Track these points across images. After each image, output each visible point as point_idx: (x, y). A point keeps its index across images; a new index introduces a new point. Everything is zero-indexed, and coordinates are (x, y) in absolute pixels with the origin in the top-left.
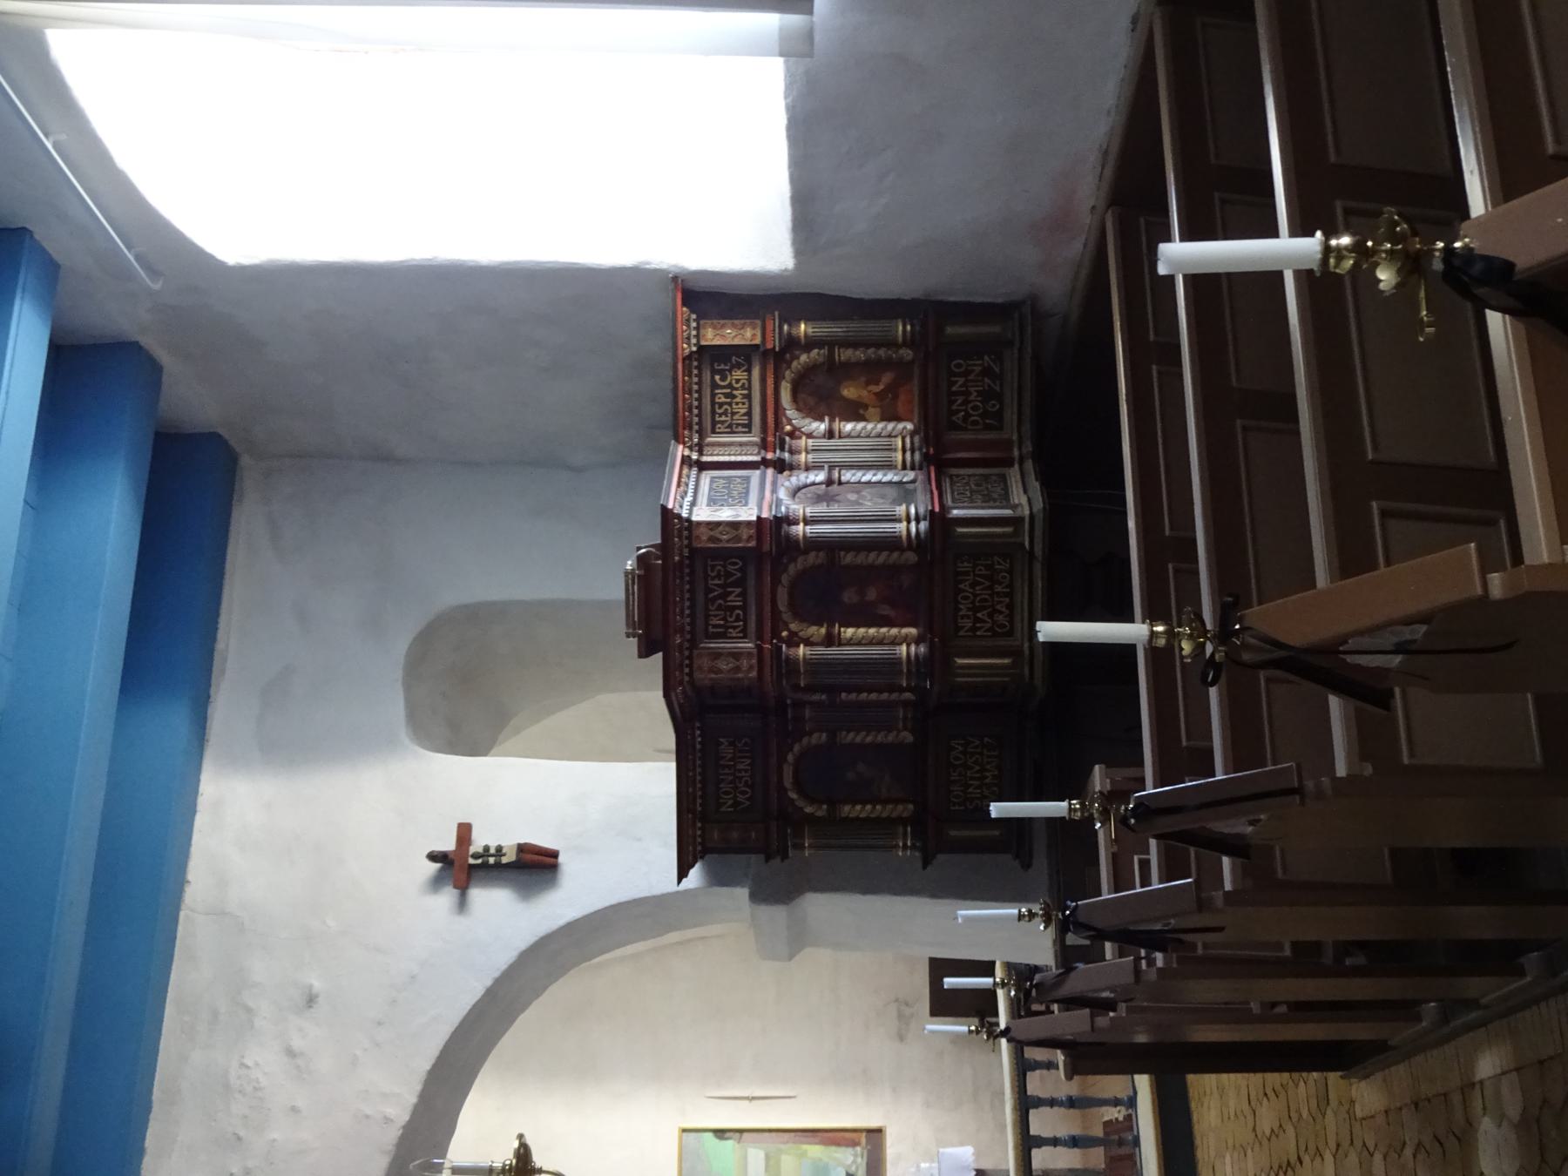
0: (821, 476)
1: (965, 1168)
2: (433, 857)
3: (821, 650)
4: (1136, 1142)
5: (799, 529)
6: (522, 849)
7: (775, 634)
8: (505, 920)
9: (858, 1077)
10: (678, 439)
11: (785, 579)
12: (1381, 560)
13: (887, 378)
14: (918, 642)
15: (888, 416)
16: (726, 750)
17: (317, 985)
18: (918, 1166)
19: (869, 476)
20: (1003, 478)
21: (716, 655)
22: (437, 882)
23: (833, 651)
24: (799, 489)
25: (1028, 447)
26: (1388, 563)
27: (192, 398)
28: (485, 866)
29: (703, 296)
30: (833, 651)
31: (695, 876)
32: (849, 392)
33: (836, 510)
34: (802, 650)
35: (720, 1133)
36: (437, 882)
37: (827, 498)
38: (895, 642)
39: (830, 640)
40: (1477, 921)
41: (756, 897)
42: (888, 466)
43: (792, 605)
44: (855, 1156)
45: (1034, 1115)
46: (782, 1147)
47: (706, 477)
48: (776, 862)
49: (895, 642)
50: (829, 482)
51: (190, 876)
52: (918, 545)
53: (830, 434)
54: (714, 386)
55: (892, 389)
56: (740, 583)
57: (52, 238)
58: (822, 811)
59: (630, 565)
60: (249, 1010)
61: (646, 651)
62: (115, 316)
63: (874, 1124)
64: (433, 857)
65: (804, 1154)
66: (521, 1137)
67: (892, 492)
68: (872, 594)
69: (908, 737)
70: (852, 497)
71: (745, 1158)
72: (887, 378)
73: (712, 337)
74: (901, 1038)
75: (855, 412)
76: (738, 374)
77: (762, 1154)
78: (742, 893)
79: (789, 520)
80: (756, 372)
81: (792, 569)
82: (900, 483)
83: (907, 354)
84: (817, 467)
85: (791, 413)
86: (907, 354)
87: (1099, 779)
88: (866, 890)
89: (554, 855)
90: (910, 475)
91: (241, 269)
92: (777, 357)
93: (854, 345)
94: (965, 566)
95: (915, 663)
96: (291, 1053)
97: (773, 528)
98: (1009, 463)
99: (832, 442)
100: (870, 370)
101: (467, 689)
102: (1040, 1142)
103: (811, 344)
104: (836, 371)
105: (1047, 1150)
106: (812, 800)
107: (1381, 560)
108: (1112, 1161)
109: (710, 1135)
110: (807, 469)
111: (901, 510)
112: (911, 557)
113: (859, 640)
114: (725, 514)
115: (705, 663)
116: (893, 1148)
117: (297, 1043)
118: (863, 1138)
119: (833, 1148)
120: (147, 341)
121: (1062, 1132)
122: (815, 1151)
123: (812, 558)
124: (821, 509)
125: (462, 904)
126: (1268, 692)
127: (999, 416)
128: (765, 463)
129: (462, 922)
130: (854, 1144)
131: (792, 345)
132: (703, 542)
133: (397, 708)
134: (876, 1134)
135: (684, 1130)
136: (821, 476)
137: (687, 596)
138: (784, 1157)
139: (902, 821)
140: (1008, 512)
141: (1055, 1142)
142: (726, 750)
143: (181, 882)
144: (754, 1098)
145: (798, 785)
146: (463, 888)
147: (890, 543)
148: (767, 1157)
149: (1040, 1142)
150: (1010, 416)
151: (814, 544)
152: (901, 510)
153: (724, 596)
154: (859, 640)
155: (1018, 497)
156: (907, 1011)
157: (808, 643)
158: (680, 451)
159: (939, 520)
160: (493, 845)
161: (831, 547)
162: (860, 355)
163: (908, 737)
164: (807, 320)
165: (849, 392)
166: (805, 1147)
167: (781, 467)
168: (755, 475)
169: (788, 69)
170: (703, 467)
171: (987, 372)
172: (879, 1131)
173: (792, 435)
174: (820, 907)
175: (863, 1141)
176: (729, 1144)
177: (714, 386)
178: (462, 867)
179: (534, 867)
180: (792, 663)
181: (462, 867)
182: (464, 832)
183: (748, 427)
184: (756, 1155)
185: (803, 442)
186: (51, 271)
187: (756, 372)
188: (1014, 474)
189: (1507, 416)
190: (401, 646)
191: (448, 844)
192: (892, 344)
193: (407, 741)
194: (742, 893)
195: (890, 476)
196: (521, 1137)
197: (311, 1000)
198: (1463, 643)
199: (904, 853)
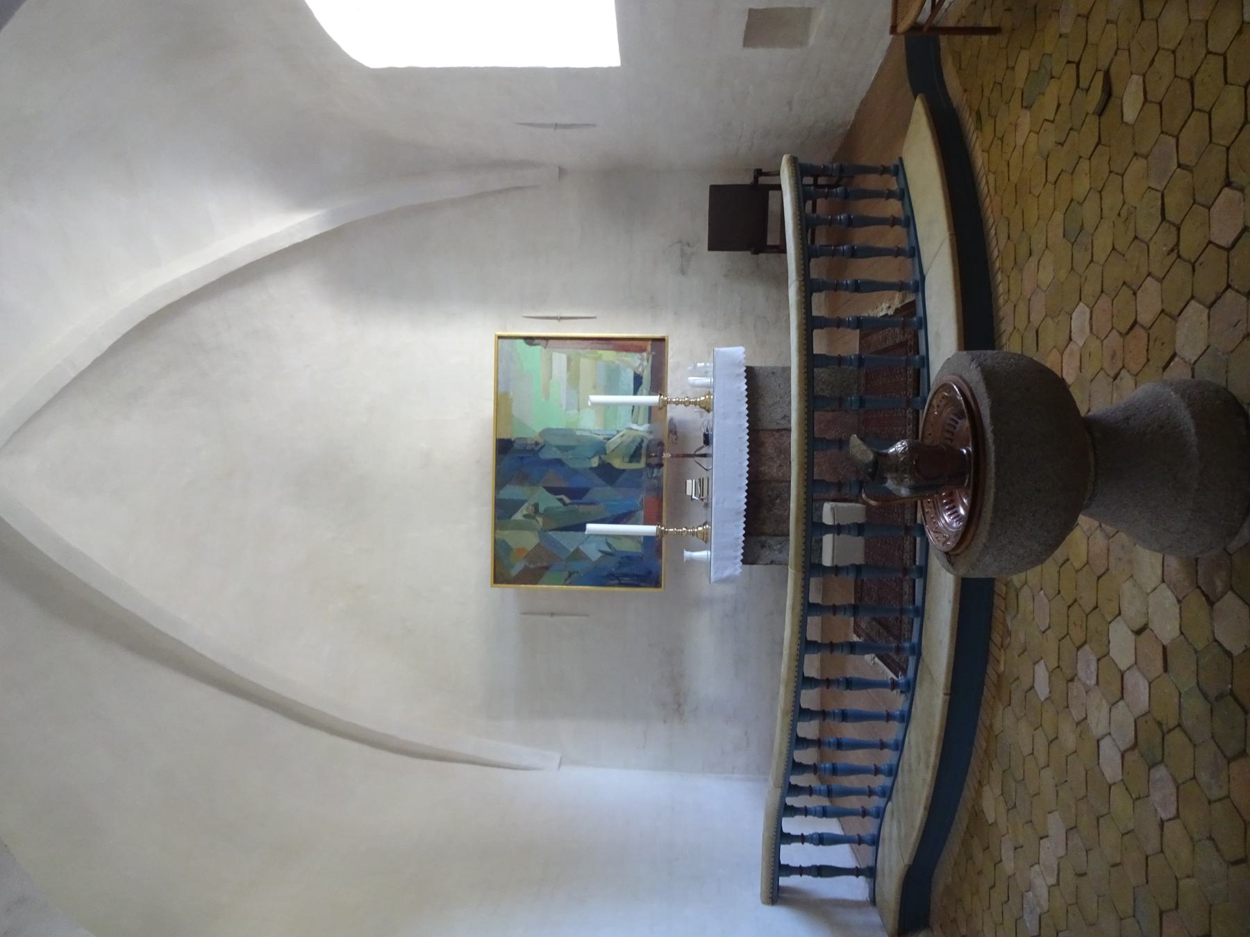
1: (739, 365)
9: (651, 303)
18: (695, 366)
35: (530, 340)
40: (1132, 225)
44: (642, 359)
45: (784, 849)
46: (581, 352)
63: (658, 335)
65: (600, 358)
71: (551, 359)
74: (683, 272)
77: (564, 357)
105: (796, 846)
109: (522, 341)
119: (624, 353)
122: (609, 355)
130: (641, 350)
134: (660, 342)
135: (500, 337)
138: (582, 360)
144: (562, 318)
148: (569, 360)
156: (688, 250)
166: (601, 352)
172: (662, 340)
175: (649, 348)
176: (537, 349)
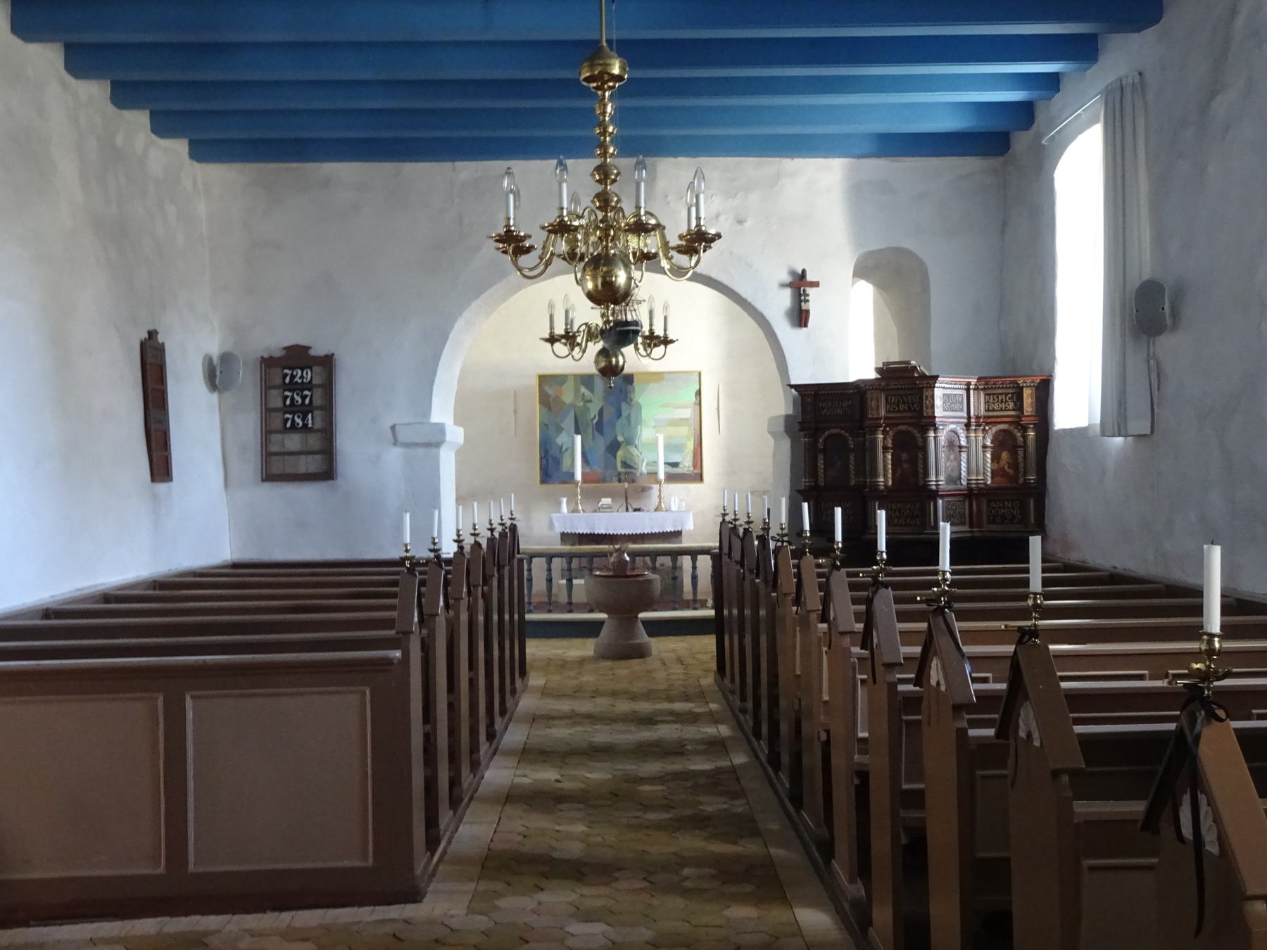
2: (804, 271)
3: (881, 445)
4: (695, 609)
5: (932, 434)
6: (808, 312)
7: (887, 425)
8: (777, 304)
10: (979, 379)
11: (911, 429)
13: (1010, 471)
14: (886, 486)
15: (993, 472)
16: (846, 404)
17: (747, 224)
19: (964, 464)
20: (963, 524)
22: (793, 273)
24: (956, 433)
25: (976, 534)
27: (1021, 141)
28: (800, 295)
29: (1044, 389)
32: (1005, 455)
34: (881, 436)
35: (699, 393)
36: (793, 273)
38: (885, 476)
39: (885, 448)
41: (787, 417)
42: (969, 472)
43: (901, 432)
47: (964, 393)
48: (798, 427)
49: (885, 476)
50: (960, 447)
51: (796, 160)
52: (926, 486)
53: (984, 447)
54: (1006, 394)
55: (1005, 474)
56: (909, 410)
58: (820, 446)
59: (913, 363)
60: (736, 195)
61: (878, 370)
62: (1040, 117)
64: (804, 271)
66: (719, 236)
67: (955, 474)
68: (905, 466)
69: (853, 482)
70: (952, 457)
72: (1010, 471)
73: (1027, 393)
75: (995, 458)
76: (1012, 405)
78: (791, 412)
79: (936, 430)
80: (1012, 413)
81: (1015, 431)
82: (960, 478)
83: (1021, 481)
84: (968, 442)
85: (994, 429)
86: (1021, 481)
88: (792, 465)
89: (806, 325)
90: (964, 483)
91: (1052, 180)
92: (1018, 423)
93: (1025, 457)
94: (918, 505)
95: (874, 486)
96: (717, 216)
97: (929, 423)
98: (971, 526)
99: (981, 449)
100: (1014, 465)
102: (694, 561)
103: (1025, 437)
104: (1013, 449)
106: (825, 441)
108: (688, 601)
110: (967, 437)
111: (942, 478)
112: (921, 483)
114: (938, 402)
115: (874, 396)
116: (693, 487)
117: (722, 218)
118: (697, 471)
121: (698, 571)
122: (690, 445)
123: (920, 440)
125: (783, 285)
127: (994, 522)
128: (969, 417)
129: (775, 286)
130: (695, 467)
131: (1025, 429)
132: (926, 393)
133: (874, 246)
134: (700, 478)
136: (963, 443)
137: (904, 387)
139: (816, 481)
141: (694, 568)
142: (846, 404)
143: (792, 157)
145: (830, 436)
146: (790, 285)
147: (926, 473)
149: (694, 561)
150: (994, 527)
151: (925, 440)
152: (942, 478)
153: (904, 403)
157: (884, 439)
158: (973, 381)
159: (934, 495)
160: (809, 298)
161: (924, 448)
162: (1021, 460)
163: (853, 482)
164: (1037, 435)
165: (1005, 455)
167: (968, 426)
170: (968, 390)
171: (1014, 517)
173: (984, 430)
174: (786, 444)
176: (693, 399)
177: (1006, 394)
178: (799, 284)
179: (800, 317)
180: (874, 432)
181: (799, 284)
182: (816, 284)
184: (688, 413)
185: (980, 435)
187: (1012, 413)
188: (966, 528)
190: (908, 244)
191: (809, 278)
192: (1025, 473)
194: (791, 412)
195: (964, 474)
196: (719, 236)
197: (740, 222)
199: (804, 482)
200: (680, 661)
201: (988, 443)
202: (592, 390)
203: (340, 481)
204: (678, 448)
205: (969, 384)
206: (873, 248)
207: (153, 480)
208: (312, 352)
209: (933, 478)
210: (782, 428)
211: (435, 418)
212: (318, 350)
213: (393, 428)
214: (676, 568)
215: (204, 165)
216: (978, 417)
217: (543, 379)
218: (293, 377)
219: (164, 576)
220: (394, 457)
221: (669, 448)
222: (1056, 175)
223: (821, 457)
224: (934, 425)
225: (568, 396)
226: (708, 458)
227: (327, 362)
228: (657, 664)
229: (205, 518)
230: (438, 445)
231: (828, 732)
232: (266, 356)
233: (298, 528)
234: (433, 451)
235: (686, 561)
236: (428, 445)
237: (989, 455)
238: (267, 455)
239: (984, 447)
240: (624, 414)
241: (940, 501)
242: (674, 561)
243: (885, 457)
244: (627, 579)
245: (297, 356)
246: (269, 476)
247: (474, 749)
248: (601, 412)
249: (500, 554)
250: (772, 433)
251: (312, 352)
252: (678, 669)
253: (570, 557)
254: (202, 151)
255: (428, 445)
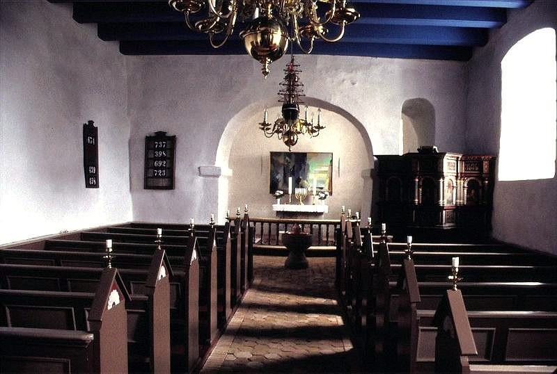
0: (455, 185)
3: (417, 184)
5: (441, 180)
12: (474, 329)
20: (453, 222)
21: (417, 164)
23: (417, 187)
26: (420, 287)
27: (479, 53)
30: (417, 187)
31: (375, 158)
33: (446, 188)
34: (417, 180)
35: (332, 161)
37: (449, 186)
41: (372, 170)
42: (456, 199)
47: (455, 162)
57: (506, 27)
62: (493, 39)
78: (373, 167)
79: (443, 178)
85: (469, 179)
87: (390, 237)
90: (454, 203)
96: (343, 81)
101: (416, 111)
107: (474, 329)
113: (419, 191)
117: (345, 82)
120: (488, 45)
121: (329, 231)
122: (328, 181)
124: (446, 184)
126: (485, 331)
128: (457, 173)
136: (455, 185)
140: (444, 222)
141: (328, 229)
152: (445, 201)
154: (419, 191)
155: (447, 225)
158: (460, 157)
159: (442, 208)
165: (473, 192)
167: (457, 177)
168: (455, 171)
169: (133, 200)
170: (457, 161)
176: (329, 163)
183: (465, 170)
185: (462, 182)
186: (500, 27)
189: (509, 366)
193: (406, 99)
194: (373, 167)
197: (353, 84)
198: (448, 344)
200: (320, 271)
201: (466, 185)
202: (290, 158)
203: (176, 190)
204: (323, 182)
205: (458, 158)
206: (411, 98)
207: (86, 187)
208: (167, 135)
209: (441, 200)
210: (369, 175)
211: (217, 164)
212: (170, 134)
213: (199, 168)
214: (320, 229)
215: (127, 56)
216: (461, 173)
217: (272, 154)
218: (159, 145)
219: (113, 226)
220: (199, 180)
221: (319, 182)
222: (503, 63)
223: (402, 189)
224: (443, 176)
225: (281, 160)
226: (334, 190)
227: (173, 140)
228: (311, 273)
229: (111, 204)
230: (218, 176)
231: (265, 73)
232: (148, 135)
233: (162, 210)
234: (216, 179)
235: (324, 226)
236: (214, 176)
237: (466, 191)
238: (146, 178)
239: (464, 187)
240: (303, 168)
241: (444, 212)
242: (320, 226)
243: (419, 190)
244: (297, 239)
245: (161, 136)
246: (147, 187)
247: (243, 284)
248: (294, 167)
249: (240, 227)
250: (363, 177)
251: (167, 135)
252: (319, 276)
253: (278, 223)
254: (126, 49)
255: (214, 176)
